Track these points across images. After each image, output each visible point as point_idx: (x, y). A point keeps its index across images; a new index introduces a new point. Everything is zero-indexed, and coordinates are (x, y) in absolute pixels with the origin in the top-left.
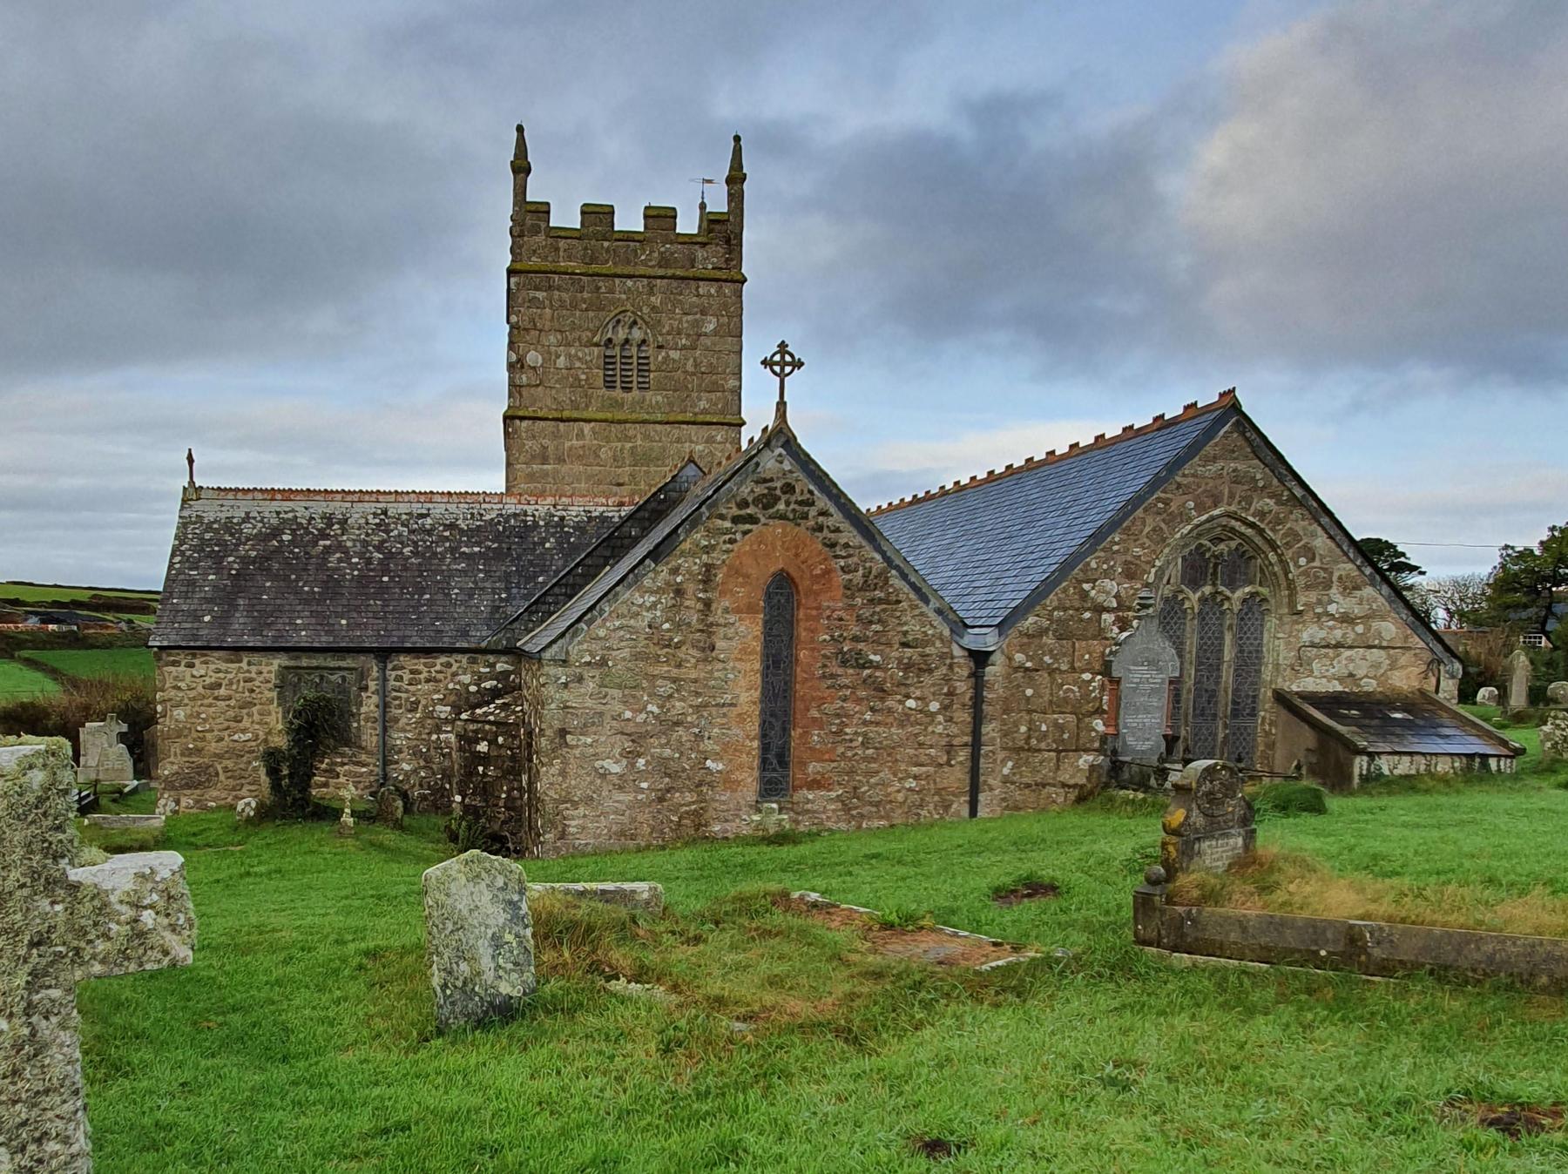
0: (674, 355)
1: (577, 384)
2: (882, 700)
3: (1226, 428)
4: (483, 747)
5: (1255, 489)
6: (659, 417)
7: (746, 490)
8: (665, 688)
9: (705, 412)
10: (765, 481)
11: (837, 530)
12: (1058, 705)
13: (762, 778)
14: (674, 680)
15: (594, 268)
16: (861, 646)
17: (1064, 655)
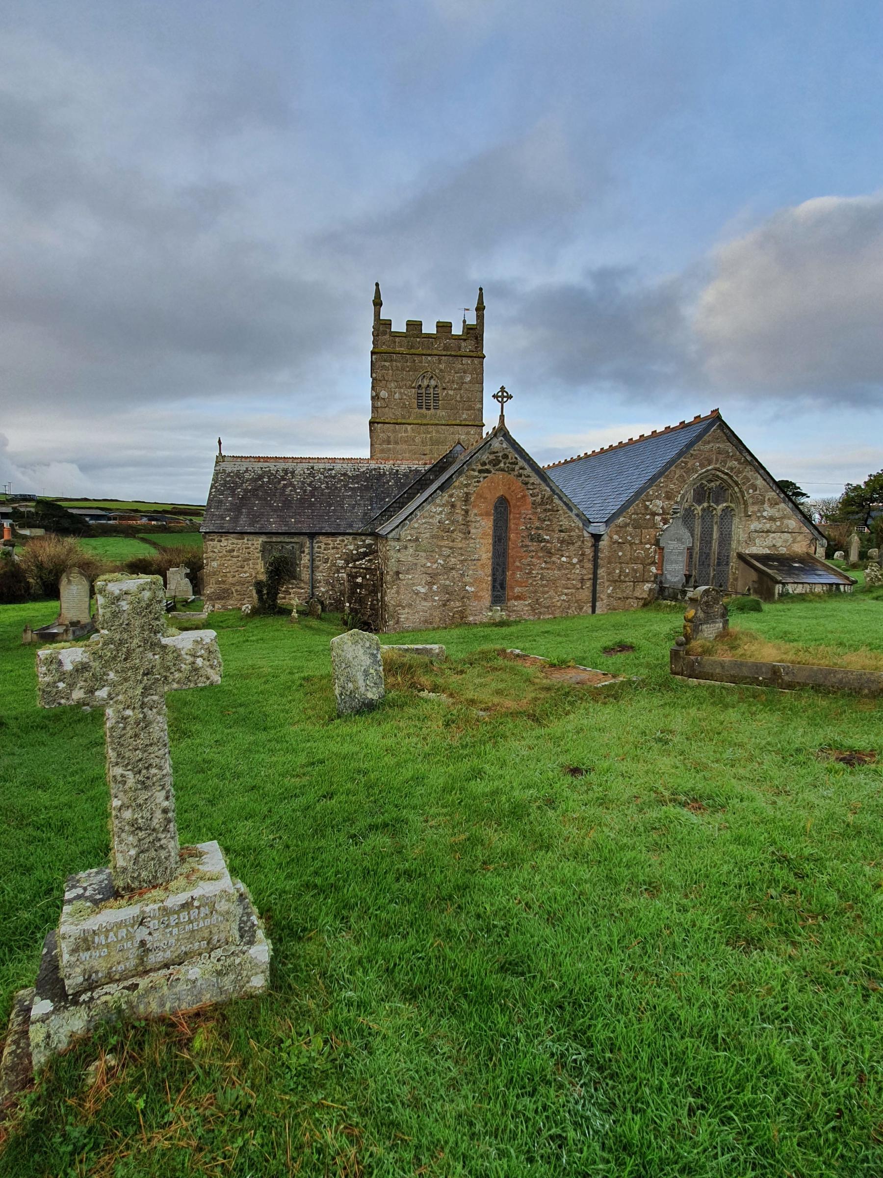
1: (404, 406)
2: (550, 557)
4: (359, 580)
5: (728, 457)
6: (444, 422)
8: (446, 552)
9: (465, 420)
10: (494, 453)
12: (634, 560)
14: (451, 548)
15: (413, 351)
16: (540, 532)
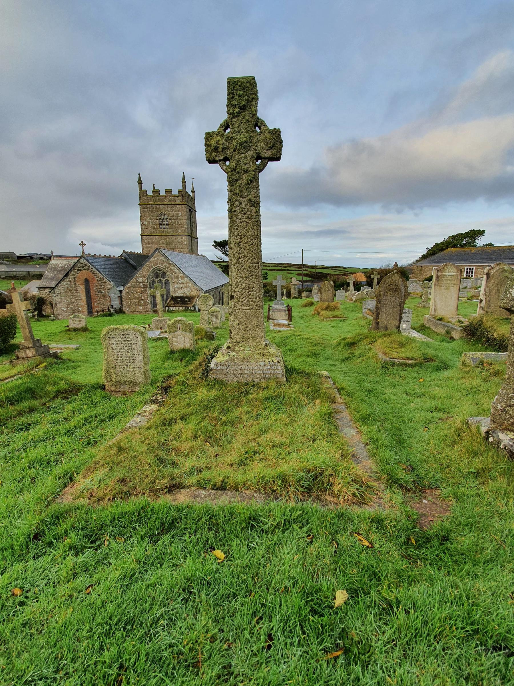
0: (173, 221)
1: (154, 228)
7: (79, 265)
8: (71, 297)
9: (180, 233)
12: (135, 298)
15: (156, 203)
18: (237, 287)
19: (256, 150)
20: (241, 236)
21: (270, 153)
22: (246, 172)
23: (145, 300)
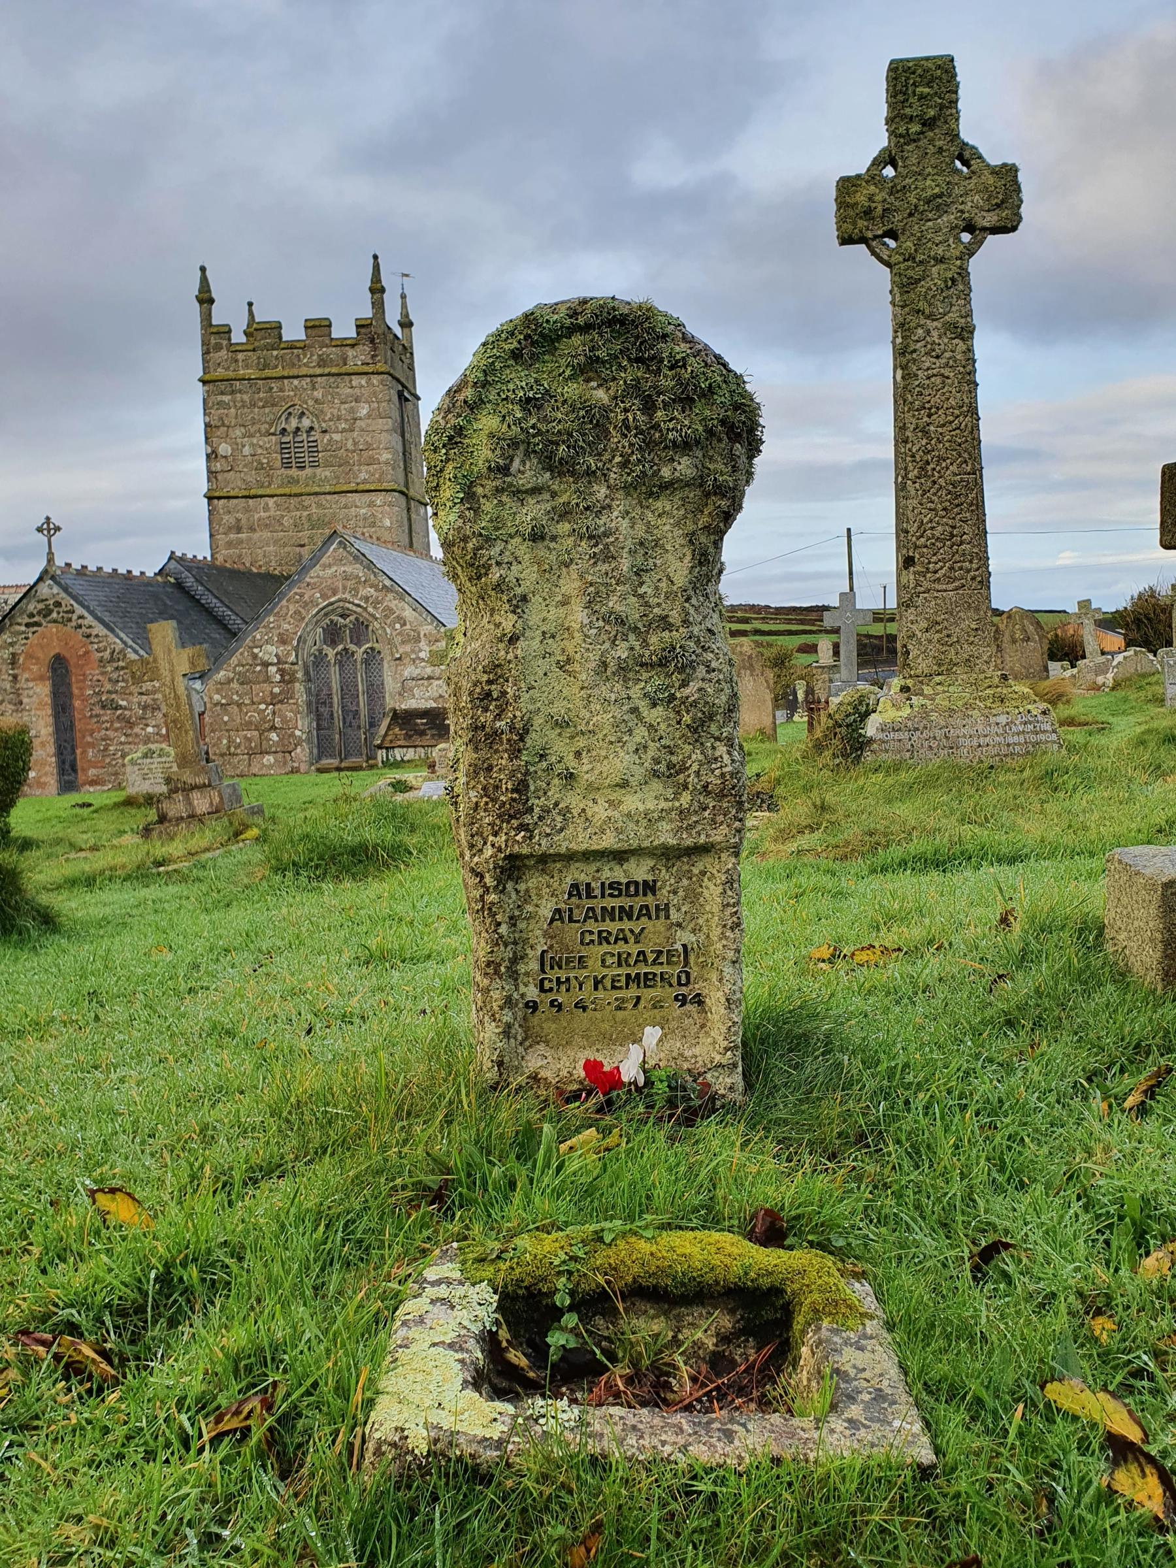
1: (260, 467)
2: (131, 728)
3: (334, 546)
5: (360, 582)
6: (328, 489)
7: (32, 607)
9: (365, 482)
10: (43, 601)
11: (90, 627)
12: (248, 725)
13: (60, 781)
15: (268, 373)
16: (114, 696)
17: (246, 694)
18: (922, 536)
19: (962, 212)
20: (930, 409)
21: (996, 218)
22: (941, 260)
23: (285, 731)
